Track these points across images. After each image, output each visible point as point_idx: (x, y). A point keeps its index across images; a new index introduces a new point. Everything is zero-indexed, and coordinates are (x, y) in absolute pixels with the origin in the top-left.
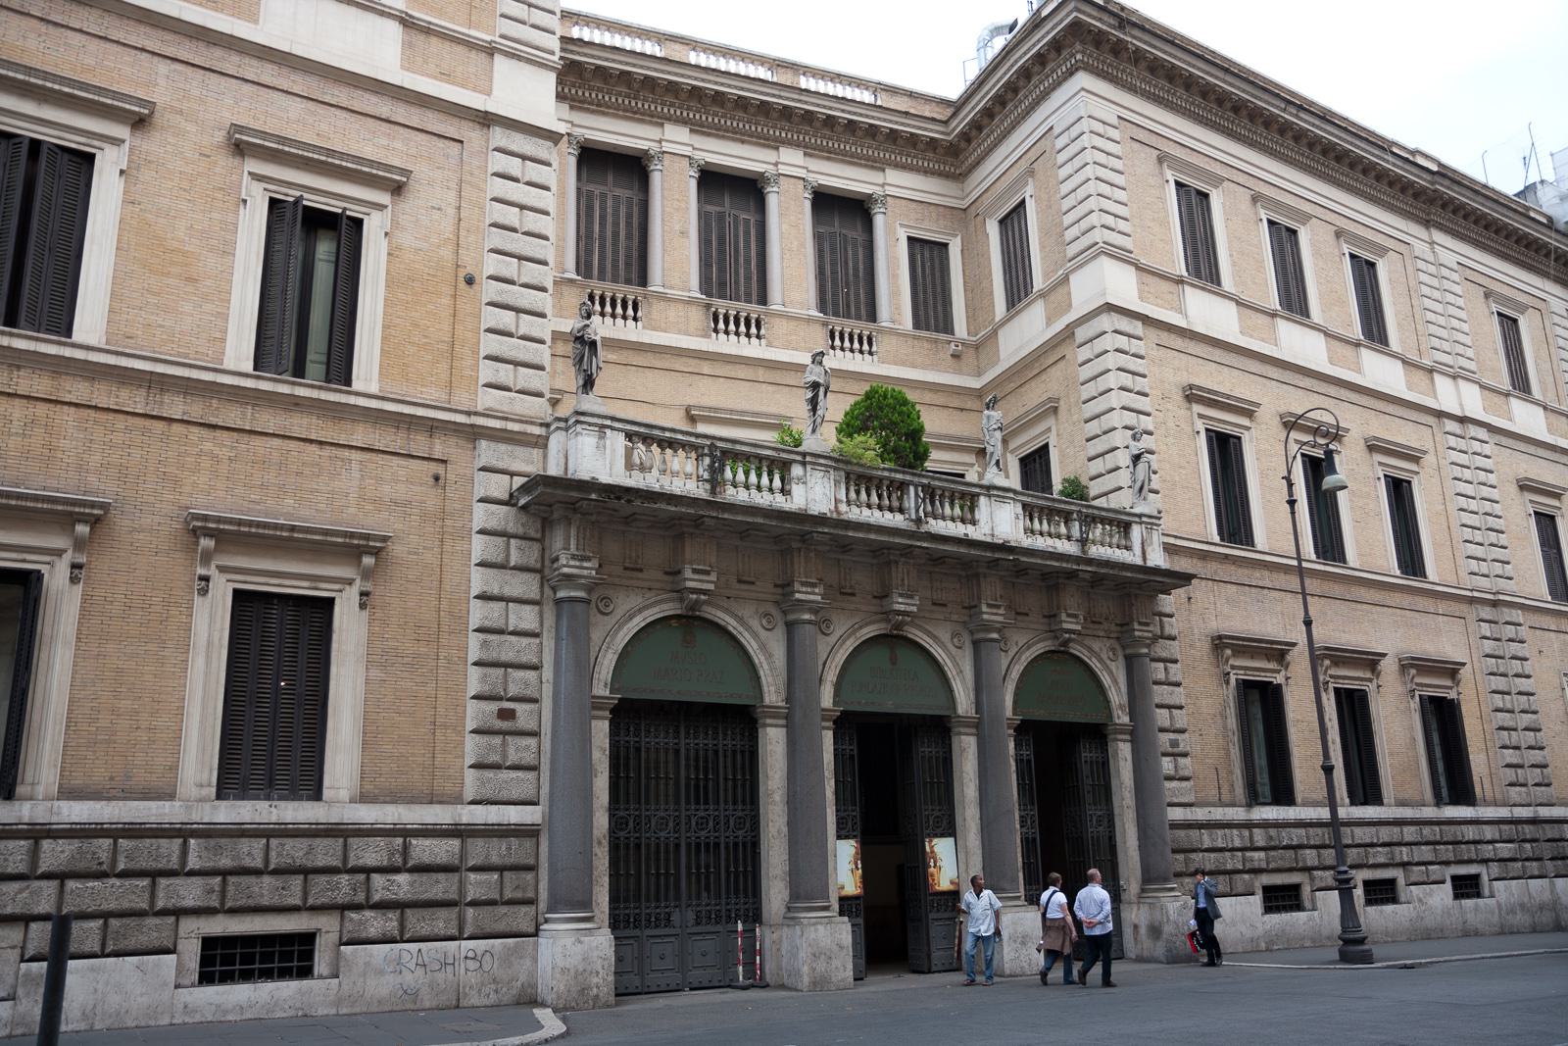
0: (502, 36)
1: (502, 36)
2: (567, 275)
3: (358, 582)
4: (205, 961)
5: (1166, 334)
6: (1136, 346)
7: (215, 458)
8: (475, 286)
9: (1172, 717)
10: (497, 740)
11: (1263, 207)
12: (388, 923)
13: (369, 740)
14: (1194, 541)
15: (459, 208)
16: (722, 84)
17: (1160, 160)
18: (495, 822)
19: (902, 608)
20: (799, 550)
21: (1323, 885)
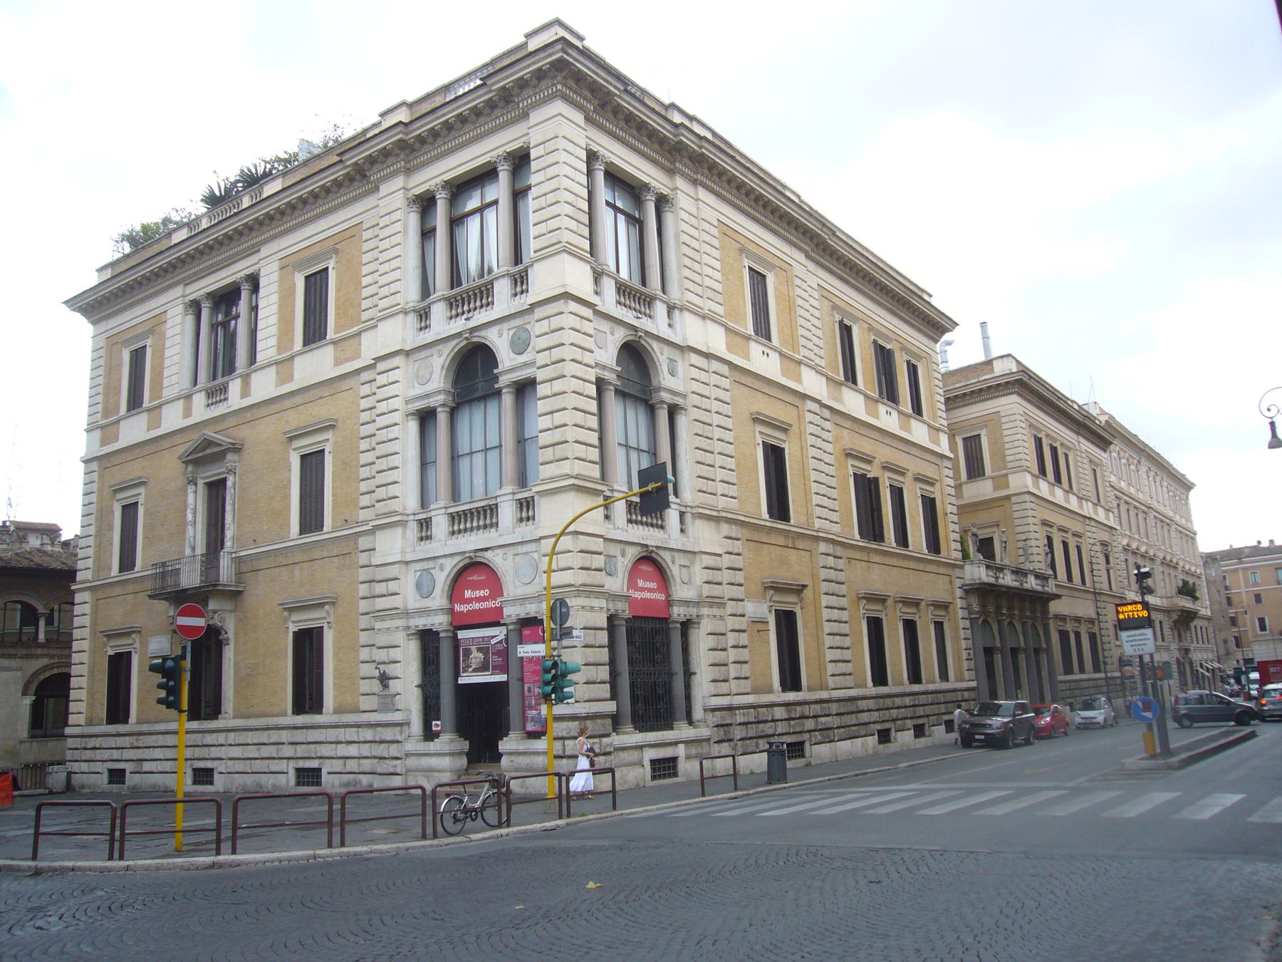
4: (653, 770)
11: (747, 257)
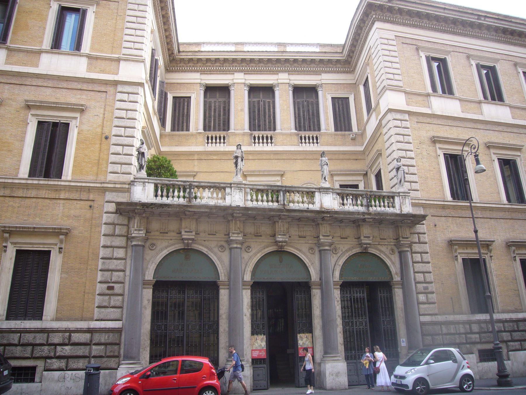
0: (124, 55)
1: (124, 55)
2: (199, 131)
3: (59, 244)
5: (421, 117)
6: (404, 124)
7: (13, 207)
8: (108, 140)
9: (424, 277)
10: (107, 298)
12: (62, 363)
13: (60, 300)
14: (436, 201)
15: (104, 114)
16: (252, 56)
17: (417, 49)
18: (103, 327)
19: (281, 240)
20: (232, 220)
21: (514, 348)
